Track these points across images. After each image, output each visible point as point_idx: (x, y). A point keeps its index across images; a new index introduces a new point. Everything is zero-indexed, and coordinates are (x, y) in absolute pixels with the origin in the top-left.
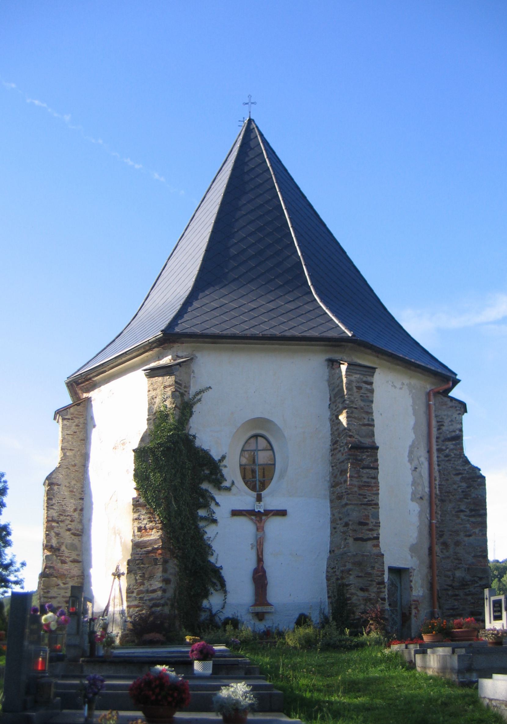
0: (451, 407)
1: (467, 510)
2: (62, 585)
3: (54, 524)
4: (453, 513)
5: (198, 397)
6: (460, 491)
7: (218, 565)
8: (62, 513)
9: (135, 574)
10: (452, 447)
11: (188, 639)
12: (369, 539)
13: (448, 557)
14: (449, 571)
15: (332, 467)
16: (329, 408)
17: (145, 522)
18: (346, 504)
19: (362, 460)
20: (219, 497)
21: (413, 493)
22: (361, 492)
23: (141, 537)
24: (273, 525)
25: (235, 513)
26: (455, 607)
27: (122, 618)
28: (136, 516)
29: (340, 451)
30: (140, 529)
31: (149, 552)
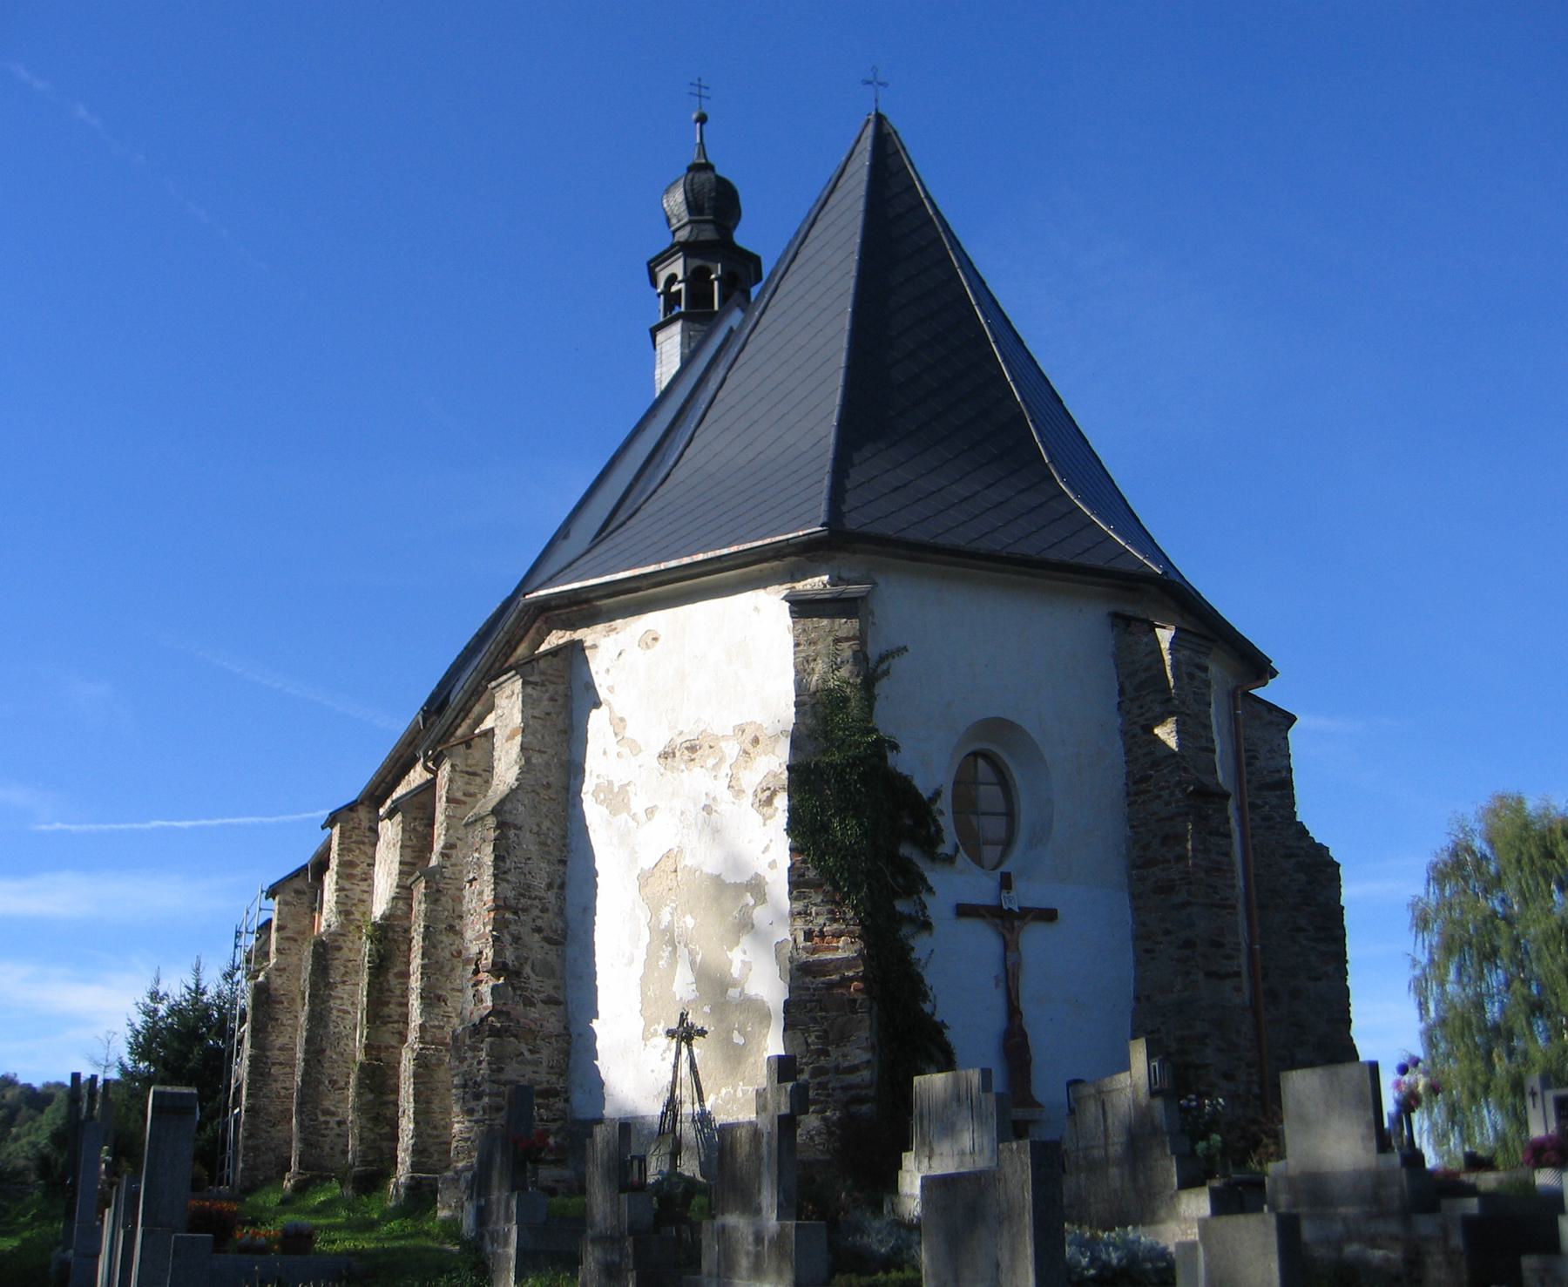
0: (1271, 723)
2: (527, 1054)
3: (508, 915)
5: (884, 666)
7: (937, 1018)
8: (525, 891)
9: (806, 1031)
10: (1274, 801)
11: (443, 1213)
12: (1228, 975)
15: (1132, 827)
16: (1119, 709)
17: (821, 920)
18: (1185, 905)
23: (814, 951)
24: (1033, 938)
25: (963, 911)
27: (700, 1131)
28: (799, 906)
29: (1159, 797)
30: (809, 935)
31: (831, 985)
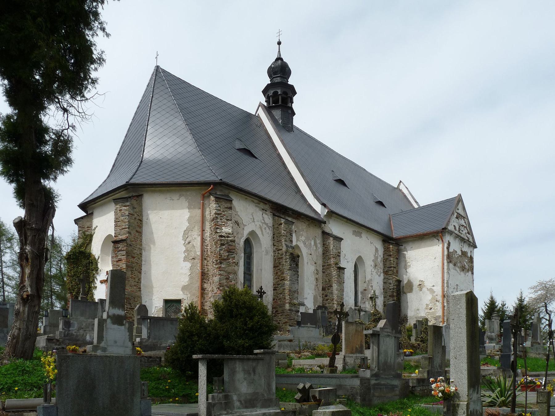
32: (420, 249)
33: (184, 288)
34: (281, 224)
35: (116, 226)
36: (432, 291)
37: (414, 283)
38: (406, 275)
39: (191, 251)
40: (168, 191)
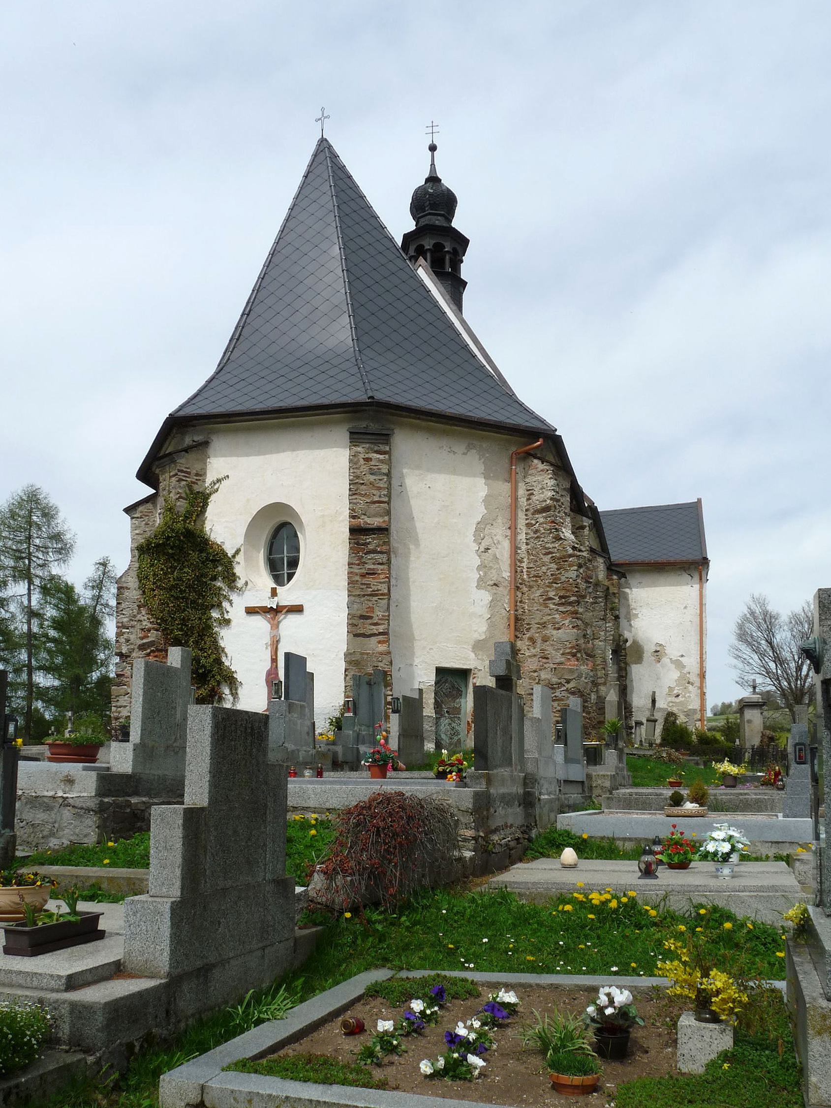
1: (557, 598)
4: (541, 601)
6: (549, 574)
10: (542, 520)
13: (535, 656)
14: (535, 671)
19: (366, 544)
20: (234, 597)
21: (481, 579)
22: (365, 581)
24: (289, 623)
25: (250, 611)
26: (812, 729)
32: (657, 589)
33: (478, 646)
34: (583, 527)
35: (353, 493)
36: (679, 665)
37: (646, 648)
38: (630, 631)
39: (491, 568)
40: (445, 433)
